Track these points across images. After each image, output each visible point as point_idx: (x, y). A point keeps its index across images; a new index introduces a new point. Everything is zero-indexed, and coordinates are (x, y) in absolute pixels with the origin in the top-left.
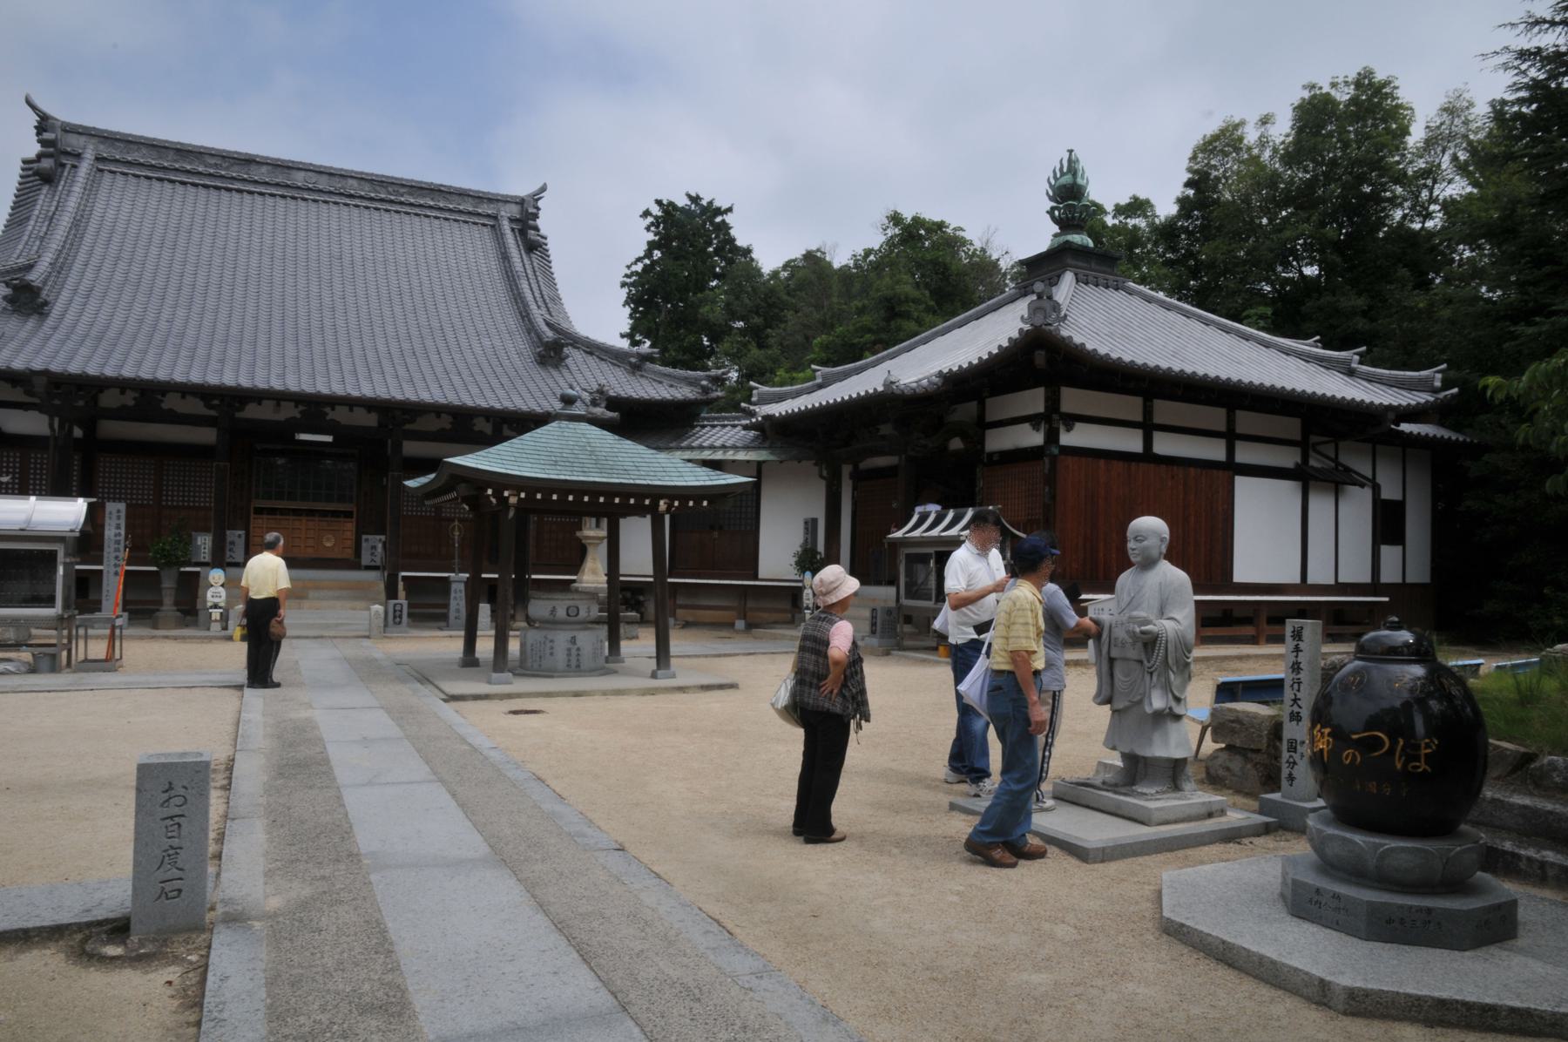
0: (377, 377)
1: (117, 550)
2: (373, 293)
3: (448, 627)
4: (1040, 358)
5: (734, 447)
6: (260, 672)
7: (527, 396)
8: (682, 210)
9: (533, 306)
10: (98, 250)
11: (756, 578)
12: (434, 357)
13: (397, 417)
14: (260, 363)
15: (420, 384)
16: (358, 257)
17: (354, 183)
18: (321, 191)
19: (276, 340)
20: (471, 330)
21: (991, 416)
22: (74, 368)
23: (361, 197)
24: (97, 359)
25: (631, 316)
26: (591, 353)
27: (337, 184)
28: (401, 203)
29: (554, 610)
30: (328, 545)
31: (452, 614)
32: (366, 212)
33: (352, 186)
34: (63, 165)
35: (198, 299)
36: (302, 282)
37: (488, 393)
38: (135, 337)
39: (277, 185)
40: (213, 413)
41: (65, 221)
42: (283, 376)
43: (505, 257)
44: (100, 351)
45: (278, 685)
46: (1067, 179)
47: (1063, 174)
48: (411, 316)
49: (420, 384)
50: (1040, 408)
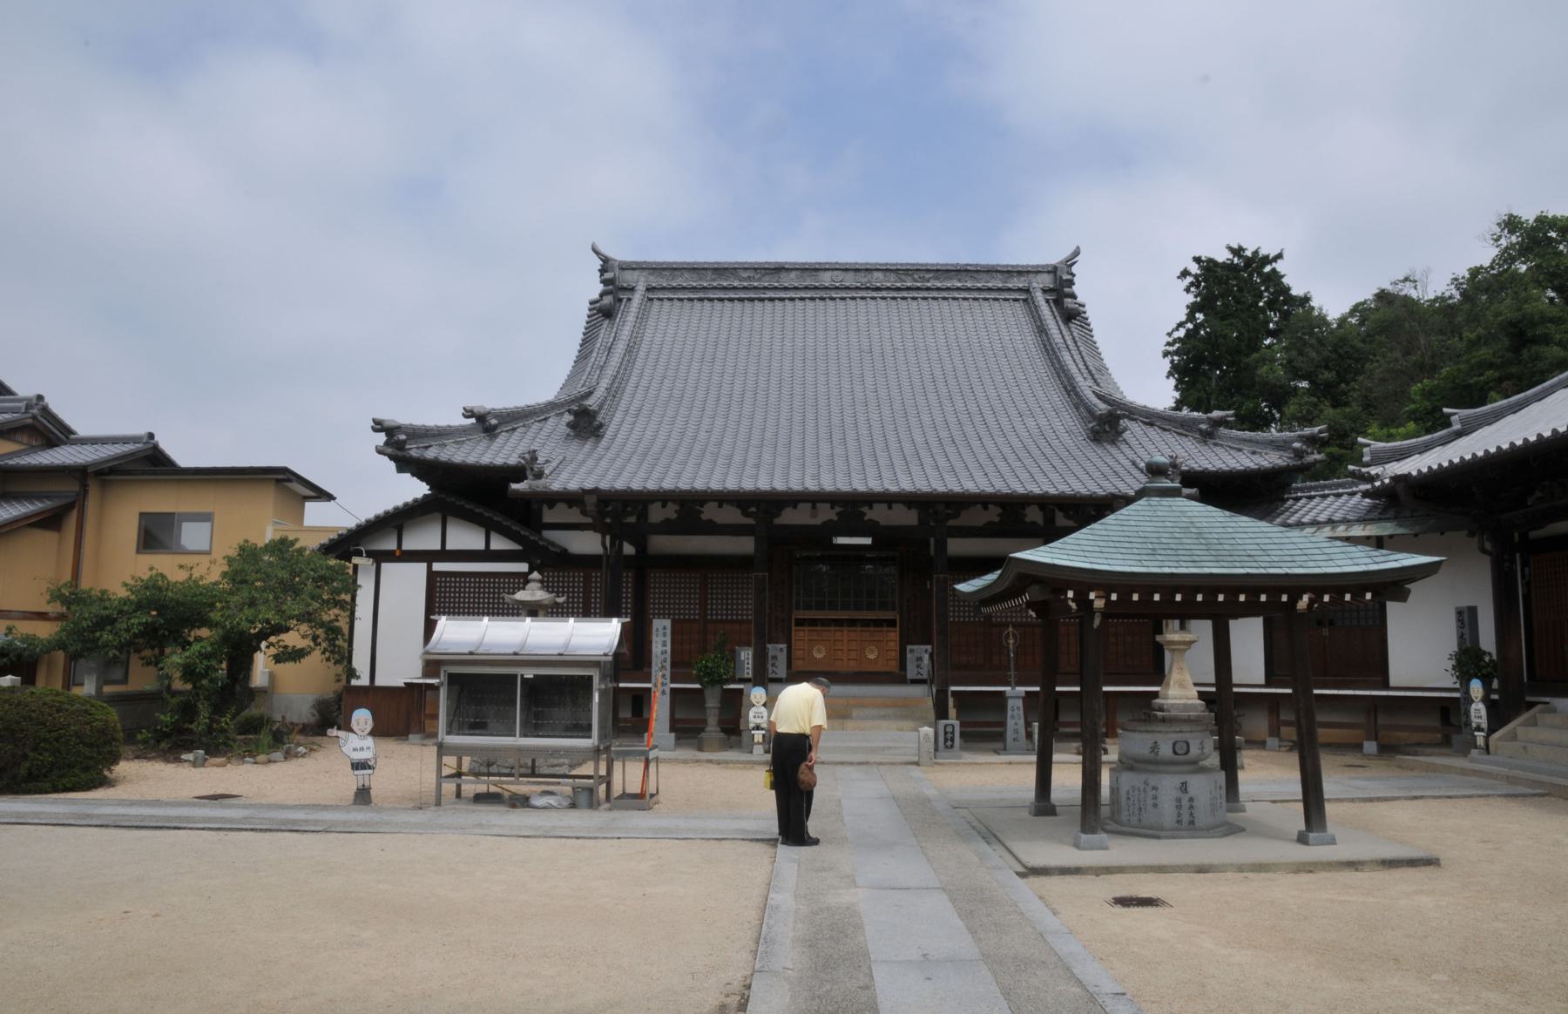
0: (915, 469)
2: (905, 383)
3: (1005, 750)
5: (1345, 521)
6: (794, 823)
7: (1084, 477)
8: (1224, 266)
9: (1079, 379)
10: (647, 372)
11: (1385, 685)
12: (975, 443)
13: (939, 510)
14: (794, 465)
15: (963, 474)
16: (888, 348)
17: (879, 275)
18: (847, 288)
19: (810, 440)
20: (1012, 411)
22: (620, 485)
23: (888, 289)
24: (642, 474)
25: (1176, 388)
26: (1152, 425)
27: (863, 279)
28: (928, 289)
30: (871, 657)
31: (1010, 735)
32: (894, 303)
33: (878, 279)
34: (620, 300)
35: (735, 408)
36: (833, 380)
37: (1039, 477)
38: (677, 449)
39: (806, 288)
40: (751, 521)
41: (620, 348)
42: (817, 476)
43: (1042, 330)
44: (645, 466)
45: (816, 842)
48: (946, 402)
49: (963, 474)
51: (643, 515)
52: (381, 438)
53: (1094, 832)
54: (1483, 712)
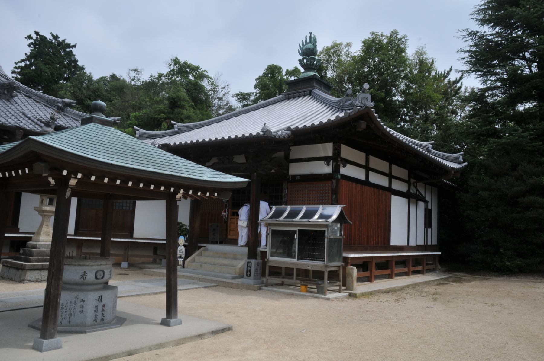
4: (363, 125)
11: (131, 237)
21: (292, 156)
26: (30, 97)
29: (84, 275)
46: (310, 46)
47: (307, 43)
50: (330, 153)
53: (52, 337)
54: (184, 250)
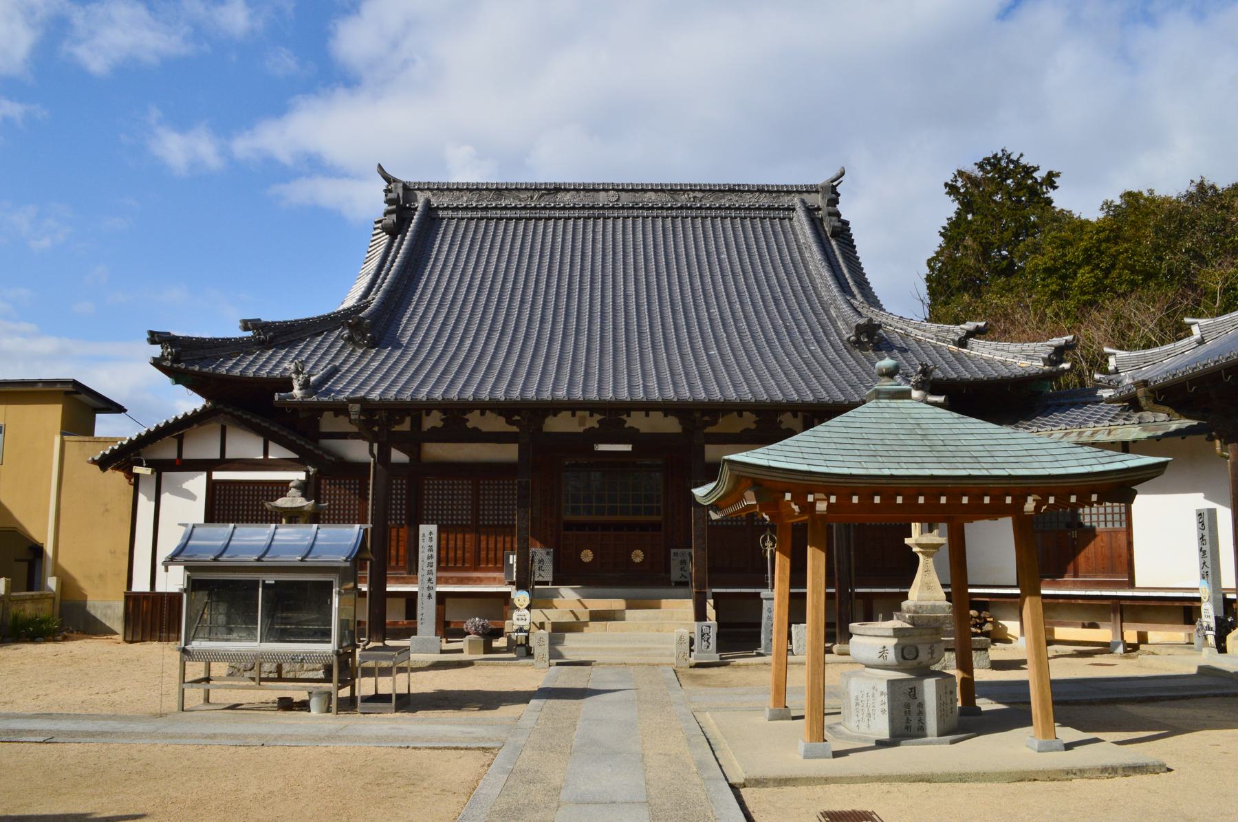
1: (430, 572)
11: (1131, 584)
30: (638, 560)
40: (515, 429)
51: (417, 423)
52: (157, 351)
